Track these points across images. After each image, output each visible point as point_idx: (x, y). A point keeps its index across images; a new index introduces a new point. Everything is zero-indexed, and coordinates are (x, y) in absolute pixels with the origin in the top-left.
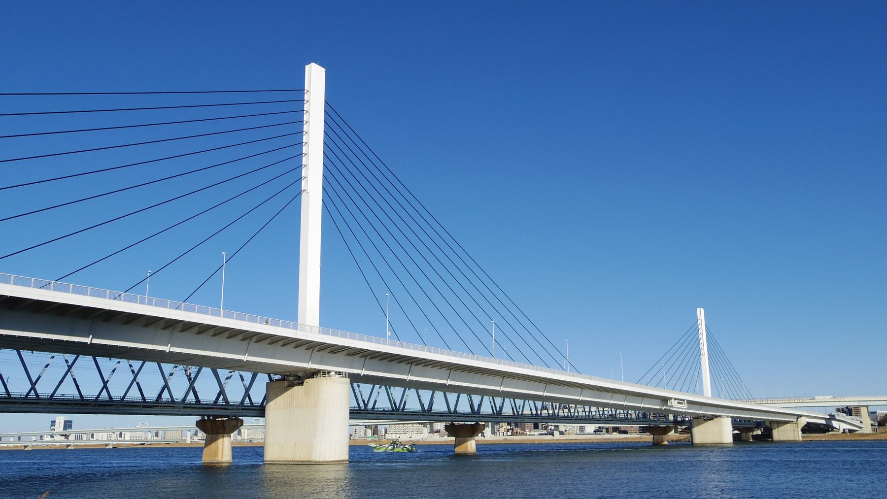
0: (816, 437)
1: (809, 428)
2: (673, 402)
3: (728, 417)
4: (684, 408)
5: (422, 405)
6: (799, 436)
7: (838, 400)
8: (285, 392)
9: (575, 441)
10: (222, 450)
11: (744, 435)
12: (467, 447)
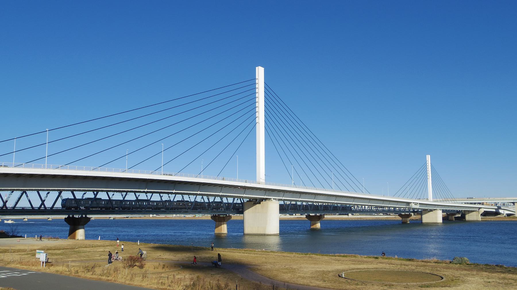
0: (489, 218)
1: (485, 214)
2: (412, 204)
3: (440, 210)
4: (418, 207)
7: (502, 199)
8: (252, 207)
9: (360, 219)
10: (224, 229)
11: (450, 217)
12: (316, 225)
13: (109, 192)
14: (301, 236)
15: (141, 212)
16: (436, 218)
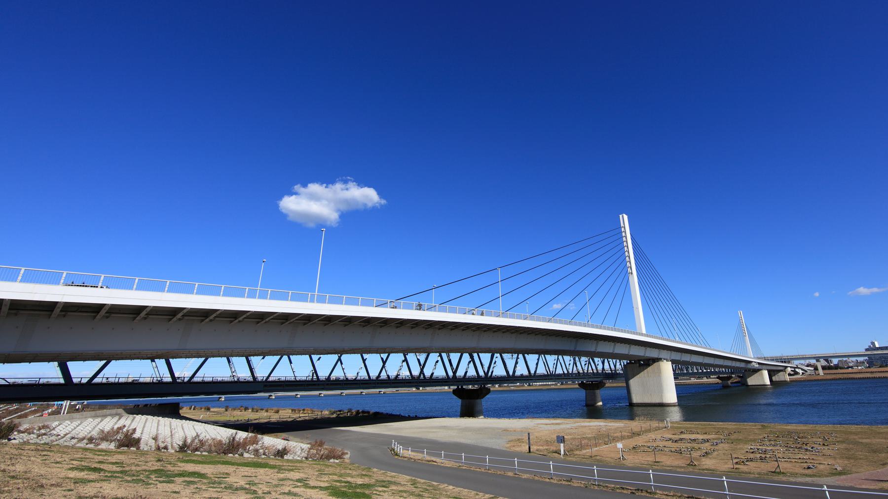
5: (507, 372)
6: (730, 384)
13: (173, 358)
14: (27, 411)
15: (509, 380)
16: (763, 378)
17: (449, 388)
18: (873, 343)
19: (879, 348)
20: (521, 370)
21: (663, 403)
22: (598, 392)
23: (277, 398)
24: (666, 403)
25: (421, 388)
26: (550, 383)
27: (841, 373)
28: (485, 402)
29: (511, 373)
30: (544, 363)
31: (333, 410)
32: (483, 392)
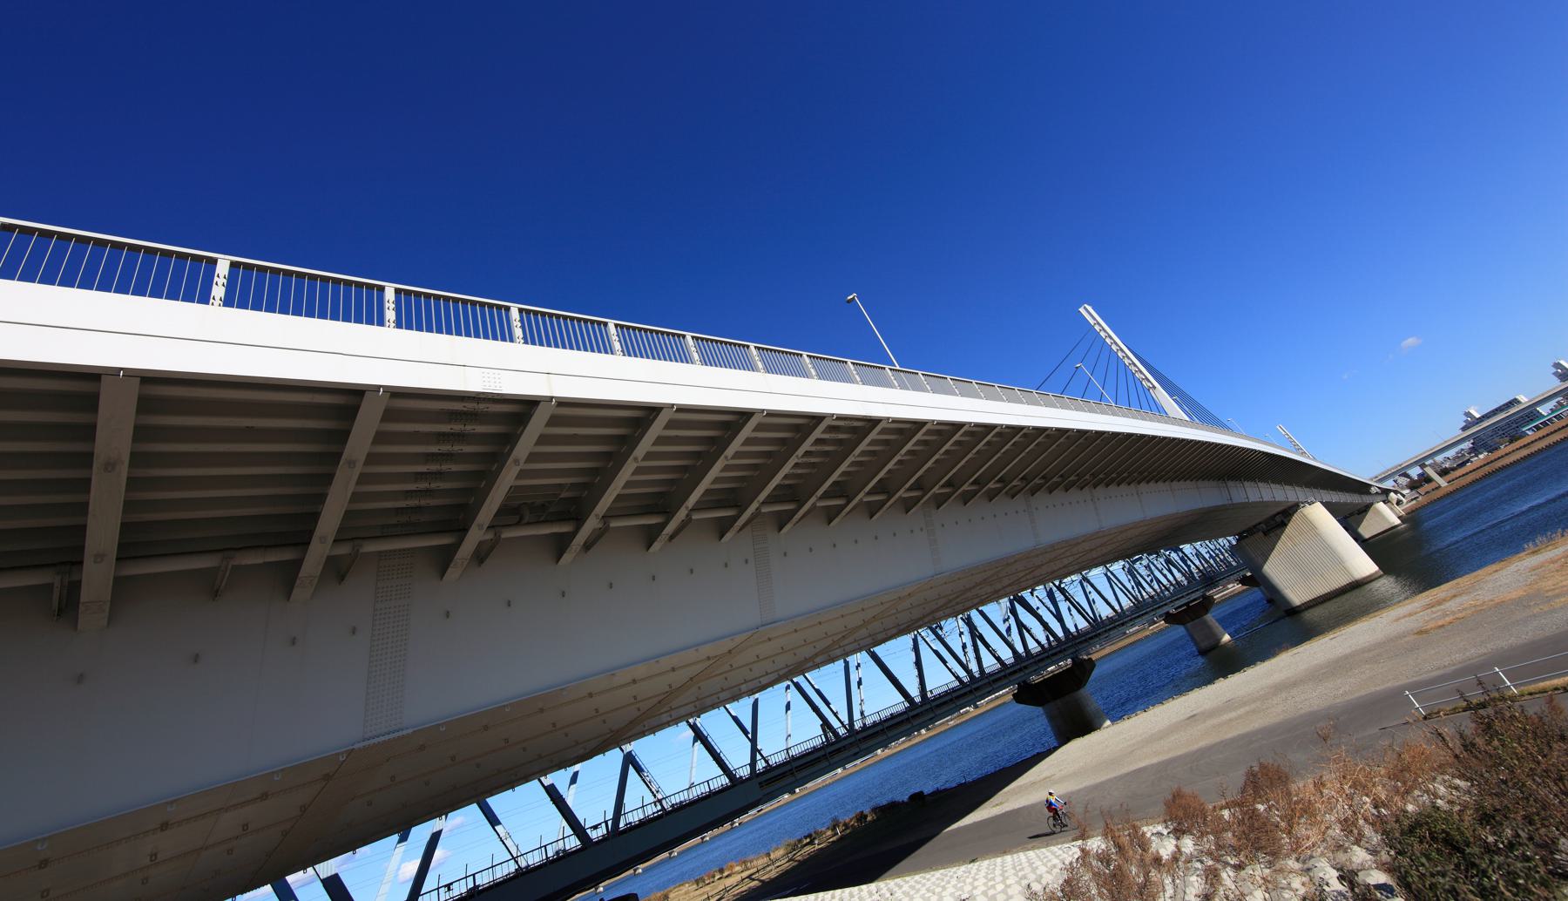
16: (1383, 517)
17: (845, 769)
18: (1468, 414)
19: (1483, 417)
20: (879, 701)
21: (1357, 581)
22: (1210, 617)
23: (645, 870)
24: (1364, 578)
25: (797, 790)
26: (1001, 693)
27: (1460, 477)
28: (1091, 694)
29: (914, 692)
30: (936, 652)
31: (792, 841)
32: (1082, 671)
